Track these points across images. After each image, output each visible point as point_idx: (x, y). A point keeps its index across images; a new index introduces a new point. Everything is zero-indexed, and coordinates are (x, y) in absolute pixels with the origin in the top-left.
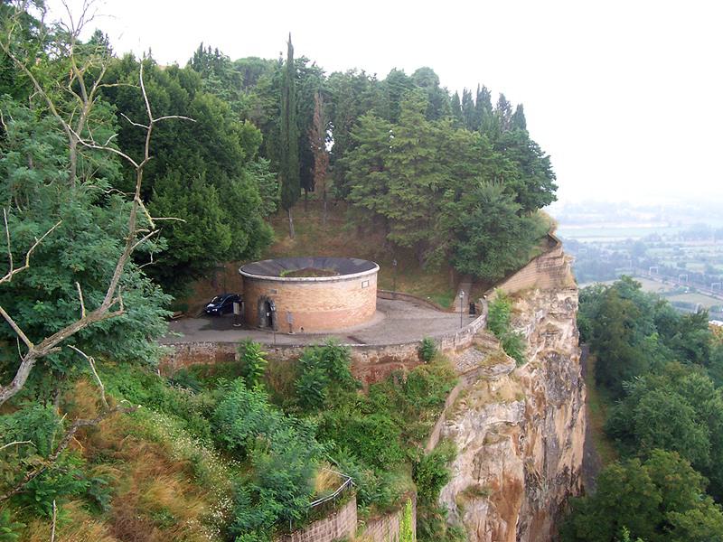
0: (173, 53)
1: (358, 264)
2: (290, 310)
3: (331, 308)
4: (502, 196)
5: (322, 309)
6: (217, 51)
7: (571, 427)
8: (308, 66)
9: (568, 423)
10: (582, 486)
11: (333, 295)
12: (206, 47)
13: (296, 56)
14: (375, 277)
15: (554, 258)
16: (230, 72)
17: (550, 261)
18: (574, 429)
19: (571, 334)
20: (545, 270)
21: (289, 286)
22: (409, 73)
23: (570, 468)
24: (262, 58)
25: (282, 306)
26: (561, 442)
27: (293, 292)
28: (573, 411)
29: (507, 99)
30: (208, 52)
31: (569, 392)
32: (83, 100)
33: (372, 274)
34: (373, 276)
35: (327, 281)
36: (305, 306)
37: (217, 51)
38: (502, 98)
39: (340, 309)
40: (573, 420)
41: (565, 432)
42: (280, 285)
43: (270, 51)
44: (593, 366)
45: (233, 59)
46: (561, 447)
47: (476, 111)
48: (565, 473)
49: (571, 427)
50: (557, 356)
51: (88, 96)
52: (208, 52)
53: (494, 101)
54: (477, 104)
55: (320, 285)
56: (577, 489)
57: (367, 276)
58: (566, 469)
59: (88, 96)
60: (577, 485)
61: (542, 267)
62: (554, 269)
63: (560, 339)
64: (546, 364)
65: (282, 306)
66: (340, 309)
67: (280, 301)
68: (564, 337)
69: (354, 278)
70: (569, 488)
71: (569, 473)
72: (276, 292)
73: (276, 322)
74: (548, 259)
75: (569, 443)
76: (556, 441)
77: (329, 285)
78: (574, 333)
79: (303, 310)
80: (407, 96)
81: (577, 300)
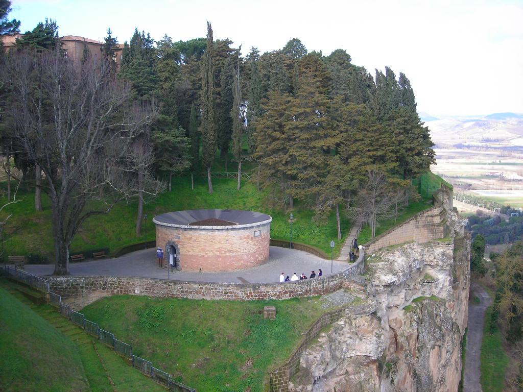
1: (256, 216)
2: (191, 253)
5: (218, 254)
6: (148, 35)
7: (444, 366)
12: (140, 31)
14: (268, 228)
15: (432, 216)
17: (429, 219)
19: (447, 283)
21: (191, 233)
25: (184, 250)
26: (435, 378)
27: (193, 238)
30: (141, 35)
33: (264, 225)
34: (266, 227)
35: (222, 229)
36: (203, 250)
37: (148, 35)
38: (402, 76)
39: (234, 254)
41: (439, 370)
42: (183, 231)
43: (187, 31)
44: (162, 383)
46: (434, 383)
47: (197, 49)
52: (141, 35)
55: (217, 233)
57: (259, 226)
61: (421, 224)
65: (184, 250)
66: (234, 254)
67: (183, 245)
69: (247, 228)
72: (179, 238)
73: (180, 263)
74: (427, 217)
75: (443, 381)
76: (430, 378)
77: (224, 233)
79: (201, 254)
80: (295, 68)
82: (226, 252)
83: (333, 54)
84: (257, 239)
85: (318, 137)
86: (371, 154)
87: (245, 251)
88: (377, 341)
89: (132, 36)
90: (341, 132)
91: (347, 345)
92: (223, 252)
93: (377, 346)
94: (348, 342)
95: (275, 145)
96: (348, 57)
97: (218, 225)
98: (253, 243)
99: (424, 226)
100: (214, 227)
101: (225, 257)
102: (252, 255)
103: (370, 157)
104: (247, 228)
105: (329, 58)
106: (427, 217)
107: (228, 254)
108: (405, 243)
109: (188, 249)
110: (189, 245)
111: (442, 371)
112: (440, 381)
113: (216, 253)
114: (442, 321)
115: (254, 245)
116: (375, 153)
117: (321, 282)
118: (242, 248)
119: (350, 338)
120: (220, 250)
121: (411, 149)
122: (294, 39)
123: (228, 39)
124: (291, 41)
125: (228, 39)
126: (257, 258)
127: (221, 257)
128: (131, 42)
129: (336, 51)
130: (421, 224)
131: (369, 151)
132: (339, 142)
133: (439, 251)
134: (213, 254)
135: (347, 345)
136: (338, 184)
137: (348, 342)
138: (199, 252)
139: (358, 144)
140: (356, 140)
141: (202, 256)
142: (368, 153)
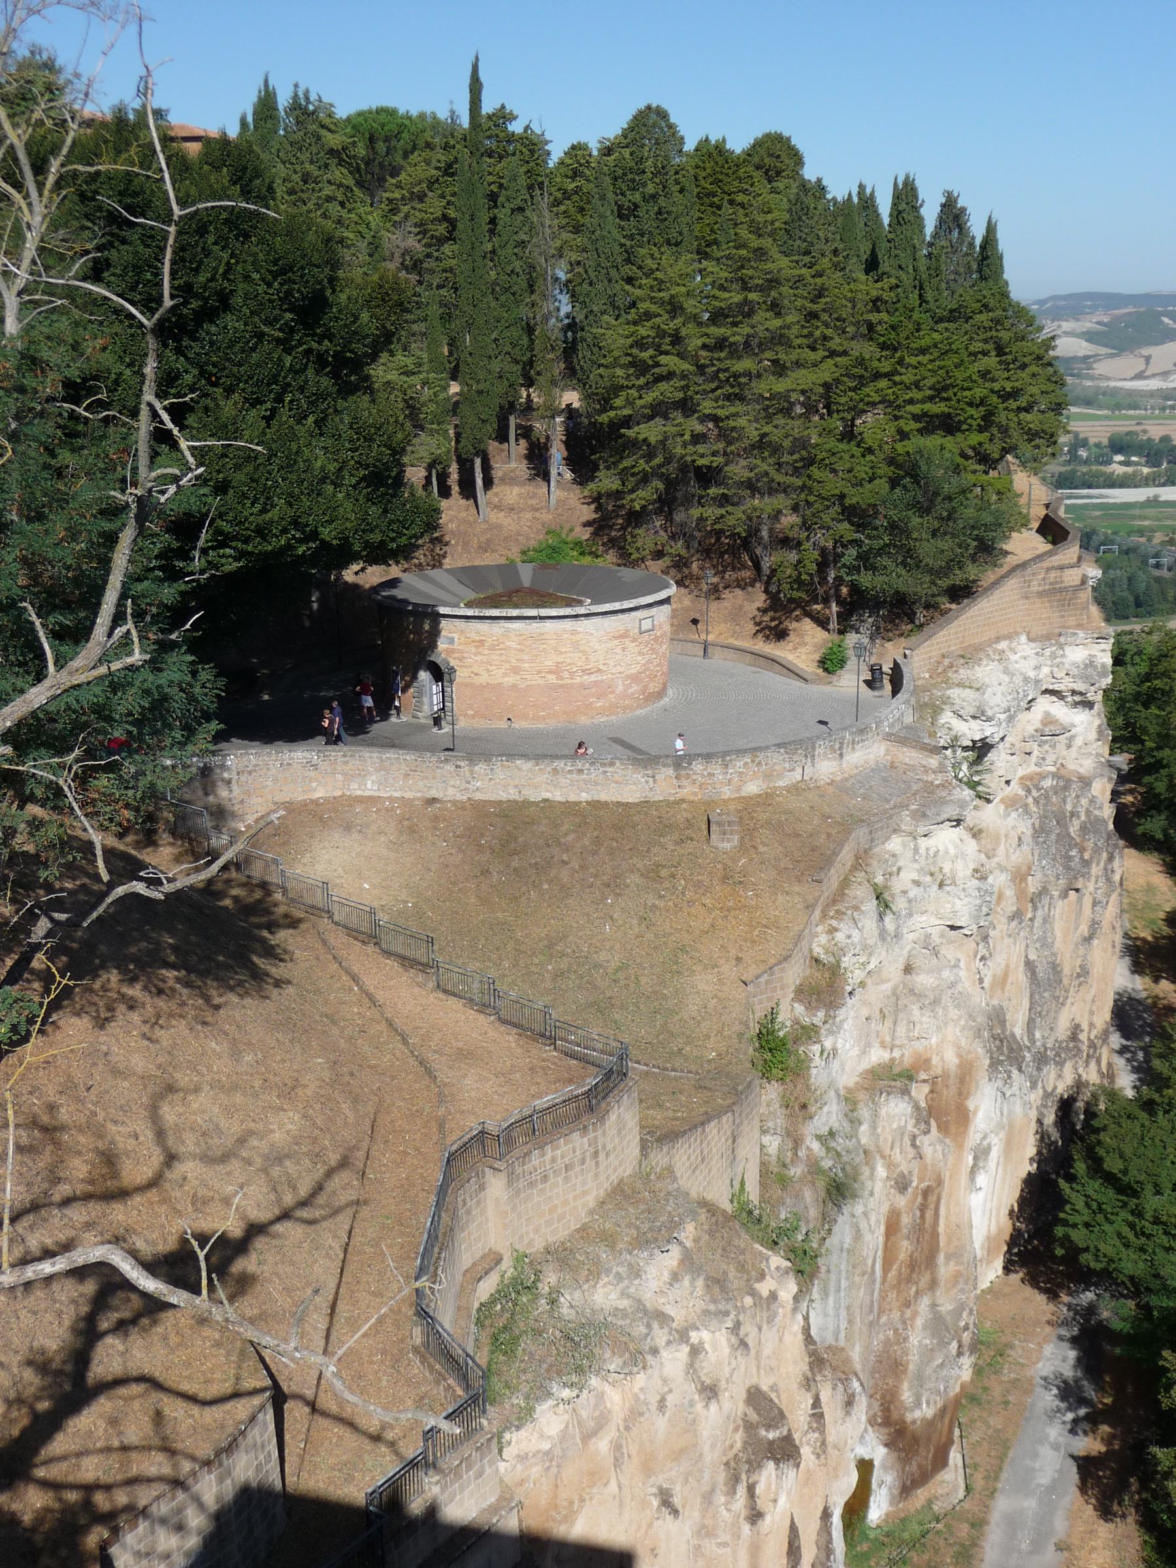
0: (208, 105)
2: (483, 679)
3: (572, 674)
4: (970, 453)
5: (552, 679)
7: (1088, 939)
8: (516, 127)
9: (1084, 929)
10: (1110, 1065)
11: (576, 646)
13: (487, 108)
15: (1062, 568)
16: (334, 140)
17: (1053, 574)
18: (1095, 942)
19: (1093, 735)
20: (1040, 594)
22: (738, 144)
23: (1085, 1026)
24: (402, 111)
26: (1067, 971)
28: (1095, 903)
29: (961, 203)
31: (1086, 863)
32: (30, 205)
39: (593, 678)
40: (1094, 926)
45: (342, 112)
46: (1066, 981)
48: (1074, 1037)
49: (1088, 939)
50: (1065, 781)
51: (27, 196)
53: (930, 214)
54: (935, 235)
55: (549, 624)
56: (1099, 1071)
58: (1076, 1030)
59: (41, 195)
60: (1099, 1062)
62: (1061, 590)
63: (1069, 746)
64: (1036, 801)
66: (593, 678)
68: (1079, 741)
69: (623, 611)
70: (1080, 1070)
71: (1083, 1037)
74: (1048, 570)
76: (1055, 968)
77: (568, 624)
78: (1100, 732)
79: (510, 680)
81: (1110, 661)
82: (572, 674)
83: (758, 144)
84: (646, 636)
85: (779, 369)
86: (916, 409)
87: (619, 669)
88: (979, 889)
89: (254, 98)
90: (833, 354)
91: (910, 901)
92: (566, 675)
93: (978, 902)
94: (911, 895)
95: (667, 390)
96: (797, 159)
97: (551, 605)
98: (636, 650)
99: (1040, 594)
100: (544, 612)
101: (572, 686)
102: (635, 678)
103: (916, 418)
104: (623, 611)
105: (749, 154)
106: (1048, 570)
107: (578, 680)
108: (998, 639)
109: (475, 669)
110: (479, 658)
111: (1081, 952)
112: (1079, 976)
113: (550, 676)
114: (1083, 829)
115: (640, 653)
116: (928, 406)
117: (837, 746)
118: (611, 663)
119: (917, 883)
120: (557, 671)
121: (1015, 394)
122: (649, 108)
123: (503, 107)
124: (640, 112)
125: (503, 107)
126: (646, 687)
127: (561, 686)
128: (255, 113)
129: (768, 136)
130: (1035, 587)
131: (911, 402)
132: (829, 380)
133: (1076, 654)
134: (540, 681)
135: (910, 901)
136: (837, 492)
137: (911, 895)
138: (505, 675)
139: (883, 383)
140: (877, 376)
141: (514, 687)
142: (909, 408)
